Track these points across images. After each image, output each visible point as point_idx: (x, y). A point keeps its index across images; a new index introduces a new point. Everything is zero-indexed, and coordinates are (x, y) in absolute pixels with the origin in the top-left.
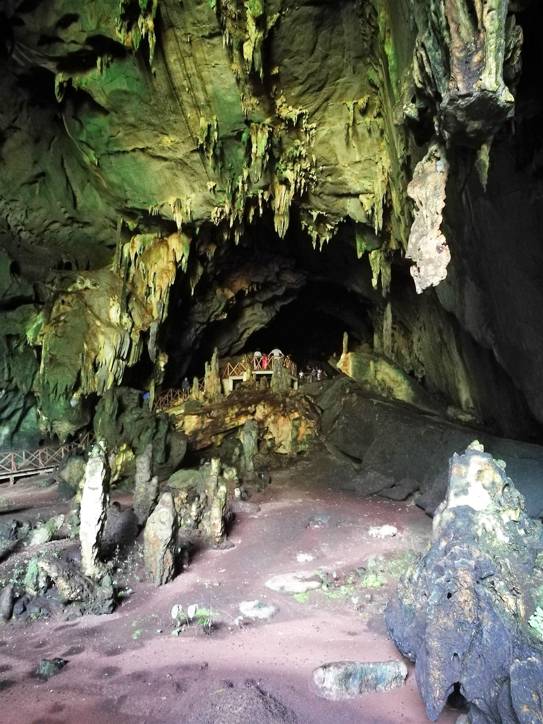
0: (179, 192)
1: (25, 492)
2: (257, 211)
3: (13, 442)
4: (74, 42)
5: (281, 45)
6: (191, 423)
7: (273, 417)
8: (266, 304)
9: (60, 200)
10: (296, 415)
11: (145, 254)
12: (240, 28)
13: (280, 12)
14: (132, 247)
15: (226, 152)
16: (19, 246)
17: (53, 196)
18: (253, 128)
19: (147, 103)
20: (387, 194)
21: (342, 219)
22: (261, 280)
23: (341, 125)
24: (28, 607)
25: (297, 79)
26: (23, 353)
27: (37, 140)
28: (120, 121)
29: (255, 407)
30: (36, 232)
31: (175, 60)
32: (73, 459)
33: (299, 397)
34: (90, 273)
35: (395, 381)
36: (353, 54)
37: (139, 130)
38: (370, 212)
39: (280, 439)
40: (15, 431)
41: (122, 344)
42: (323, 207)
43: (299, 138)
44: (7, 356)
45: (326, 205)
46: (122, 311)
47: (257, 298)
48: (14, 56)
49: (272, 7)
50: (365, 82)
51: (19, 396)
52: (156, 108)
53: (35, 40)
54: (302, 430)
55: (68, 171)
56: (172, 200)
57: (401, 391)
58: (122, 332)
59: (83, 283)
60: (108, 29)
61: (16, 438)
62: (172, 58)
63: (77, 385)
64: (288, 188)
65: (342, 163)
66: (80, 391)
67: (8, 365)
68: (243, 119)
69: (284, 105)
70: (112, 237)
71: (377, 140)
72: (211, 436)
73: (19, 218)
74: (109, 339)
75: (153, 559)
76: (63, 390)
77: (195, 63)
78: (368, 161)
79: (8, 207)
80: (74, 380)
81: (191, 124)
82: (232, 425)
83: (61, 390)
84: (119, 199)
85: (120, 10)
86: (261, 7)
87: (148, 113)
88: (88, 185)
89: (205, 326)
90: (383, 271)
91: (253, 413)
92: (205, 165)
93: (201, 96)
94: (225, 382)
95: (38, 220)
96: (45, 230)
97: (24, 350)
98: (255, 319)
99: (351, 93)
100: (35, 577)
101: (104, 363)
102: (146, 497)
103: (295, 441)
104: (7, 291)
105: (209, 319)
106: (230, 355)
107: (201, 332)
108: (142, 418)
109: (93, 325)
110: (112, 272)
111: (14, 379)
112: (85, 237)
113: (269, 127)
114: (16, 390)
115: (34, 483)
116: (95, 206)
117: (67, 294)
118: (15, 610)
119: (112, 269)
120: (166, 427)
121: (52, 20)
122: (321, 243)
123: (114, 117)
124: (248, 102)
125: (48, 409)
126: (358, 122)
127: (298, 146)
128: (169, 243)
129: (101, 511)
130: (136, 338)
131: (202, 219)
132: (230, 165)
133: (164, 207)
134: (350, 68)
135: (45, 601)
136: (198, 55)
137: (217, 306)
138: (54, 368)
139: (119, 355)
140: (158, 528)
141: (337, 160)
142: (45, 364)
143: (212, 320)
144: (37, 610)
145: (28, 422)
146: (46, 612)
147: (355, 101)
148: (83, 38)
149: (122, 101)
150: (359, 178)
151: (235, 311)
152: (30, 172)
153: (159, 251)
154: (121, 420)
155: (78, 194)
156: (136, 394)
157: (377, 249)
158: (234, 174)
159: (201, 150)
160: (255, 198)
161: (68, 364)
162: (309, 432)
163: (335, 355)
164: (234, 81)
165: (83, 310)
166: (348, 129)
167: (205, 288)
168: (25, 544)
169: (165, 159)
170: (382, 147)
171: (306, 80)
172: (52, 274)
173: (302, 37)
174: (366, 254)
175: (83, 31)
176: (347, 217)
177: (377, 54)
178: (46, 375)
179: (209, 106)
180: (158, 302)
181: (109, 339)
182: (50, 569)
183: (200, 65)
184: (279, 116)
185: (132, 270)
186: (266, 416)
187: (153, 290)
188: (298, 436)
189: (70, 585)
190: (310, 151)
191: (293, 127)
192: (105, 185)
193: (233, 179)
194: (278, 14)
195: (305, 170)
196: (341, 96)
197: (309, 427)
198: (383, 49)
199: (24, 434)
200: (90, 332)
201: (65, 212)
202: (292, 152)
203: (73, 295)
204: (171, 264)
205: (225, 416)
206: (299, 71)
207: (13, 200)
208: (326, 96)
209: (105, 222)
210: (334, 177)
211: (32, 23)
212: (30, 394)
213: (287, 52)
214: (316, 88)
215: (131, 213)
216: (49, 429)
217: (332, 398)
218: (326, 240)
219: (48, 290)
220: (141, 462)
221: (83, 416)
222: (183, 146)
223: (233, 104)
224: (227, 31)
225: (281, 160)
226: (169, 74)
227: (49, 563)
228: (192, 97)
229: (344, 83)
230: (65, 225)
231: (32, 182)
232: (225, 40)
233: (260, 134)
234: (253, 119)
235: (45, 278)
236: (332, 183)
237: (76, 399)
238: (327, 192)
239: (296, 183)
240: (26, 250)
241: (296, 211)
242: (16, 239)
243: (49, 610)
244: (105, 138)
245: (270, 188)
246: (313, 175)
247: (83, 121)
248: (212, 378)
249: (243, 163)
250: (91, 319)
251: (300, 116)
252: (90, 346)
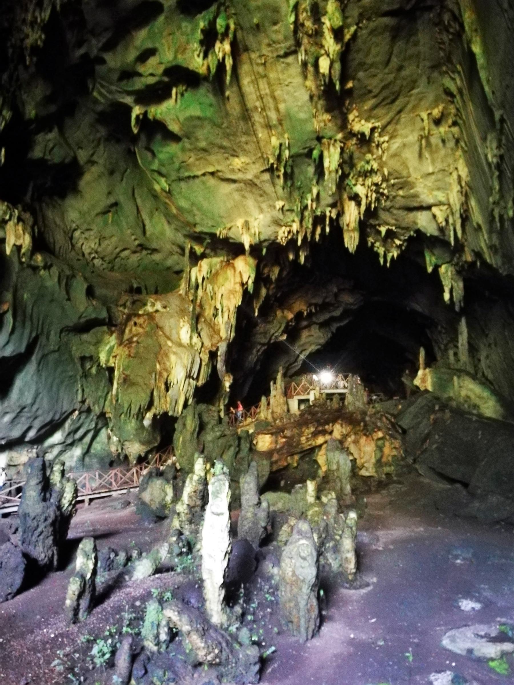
0: (248, 213)
1: (100, 514)
2: (323, 229)
3: (85, 463)
4: (152, 75)
5: (357, 57)
6: (264, 442)
7: (353, 437)
8: (323, 325)
9: (131, 227)
10: (380, 434)
11: (213, 277)
12: (316, 44)
13: (357, 24)
14: (200, 271)
15: (296, 171)
16: (93, 272)
17: (124, 224)
18: (324, 144)
19: (219, 126)
20: (465, 204)
21: (412, 233)
22: (319, 300)
23: (414, 137)
24: (149, 667)
25: (370, 92)
26: (96, 375)
27: (112, 173)
28: (192, 147)
29: (333, 425)
30: (107, 259)
31: (249, 83)
32: (155, 480)
33: (379, 416)
34: (159, 297)
35: (479, 397)
36: (428, 64)
37: (210, 154)
38: (444, 224)
39: (363, 461)
40: (87, 452)
41: (192, 363)
42: (393, 222)
43: (370, 152)
44: (81, 377)
45: (396, 220)
46: (192, 331)
47: (314, 319)
48: (95, 94)
49: (349, 20)
50: (441, 91)
51: (91, 417)
52: (228, 130)
53: (115, 76)
54: (387, 450)
55: (139, 201)
56: (240, 222)
57: (488, 408)
58: (193, 352)
59: (153, 305)
60: (185, 59)
61: (87, 459)
62: (246, 81)
63: (151, 404)
64: (359, 204)
65: (414, 176)
66: (153, 411)
67: (82, 386)
68: (315, 136)
69: (356, 119)
70: (178, 263)
71: (452, 149)
72: (287, 457)
73: (92, 245)
74: (181, 358)
75: (292, 604)
76: (137, 410)
77: (269, 83)
78: (441, 172)
79: (83, 236)
80: (148, 399)
81: (262, 144)
82: (309, 445)
83: (135, 410)
84: (188, 224)
85: (199, 35)
86: (340, 18)
87: (219, 137)
88: (157, 213)
89: (266, 347)
90: (455, 285)
91: (331, 433)
92: (274, 184)
93: (273, 116)
94: (290, 401)
95: (110, 248)
96: (116, 258)
97: (97, 372)
98: (312, 339)
99: (424, 104)
100: (155, 627)
101: (175, 383)
102: (255, 523)
103: (379, 463)
104: (83, 313)
105: (270, 339)
106: (293, 375)
107: (262, 353)
108: (225, 436)
109: (164, 346)
110: (180, 295)
111: (87, 401)
112: (154, 263)
113: (341, 142)
114: (89, 411)
115: (109, 504)
116: (163, 233)
117: (139, 316)
118: (135, 672)
119: (181, 292)
120: (248, 445)
121: (132, 55)
122: (389, 259)
123: (186, 144)
124: (320, 118)
125: (120, 430)
126: (432, 132)
127: (370, 160)
128: (236, 265)
129: (228, 542)
130: (206, 357)
131: (269, 240)
132: (299, 183)
133: (233, 229)
134: (424, 79)
135: (169, 659)
136: (272, 75)
137: (278, 328)
138: (127, 387)
139: (190, 374)
140: (298, 564)
141: (409, 172)
142: (118, 384)
143: (272, 341)
144: (161, 673)
145: (98, 443)
146: (172, 677)
147: (429, 112)
148: (161, 69)
149: (195, 127)
150: (432, 190)
151: (293, 332)
152: (105, 202)
153: (226, 272)
154: (202, 438)
155: (147, 222)
156: (215, 411)
157: (447, 263)
158: (303, 193)
159: (271, 170)
160: (324, 216)
161: (142, 383)
162: (395, 453)
163: (407, 372)
164: (307, 97)
165: (155, 332)
166: (421, 141)
167: (267, 310)
168: (127, 577)
169: (234, 181)
170: (457, 157)
171: (380, 92)
172: (125, 298)
173: (377, 49)
174: (437, 267)
175: (161, 63)
176: (418, 231)
177: (454, 61)
178: (120, 395)
179: (281, 124)
180: (227, 323)
181: (181, 358)
182: (180, 620)
183: (274, 85)
184: (351, 130)
185: (200, 292)
186: (345, 437)
187: (220, 311)
188: (382, 457)
189: (206, 642)
190: (382, 165)
191: (365, 141)
192: (174, 211)
193: (302, 197)
194: (355, 27)
195: (376, 185)
196: (414, 108)
197: (395, 448)
198: (470, 49)
199: (95, 455)
200: (162, 352)
201: (135, 239)
202: (363, 166)
203: (146, 317)
204: (238, 285)
205: (301, 435)
206: (374, 84)
207: (88, 230)
208: (398, 109)
209: (172, 248)
210: (405, 190)
211: (114, 61)
212: (102, 415)
213: (362, 64)
214: (389, 100)
215: (198, 238)
216: (120, 451)
217: (416, 416)
218: (393, 256)
219: (121, 313)
220: (246, 482)
221: (153, 436)
222: (253, 166)
223: (305, 121)
224: (303, 48)
225: (352, 175)
226: (242, 95)
227: (179, 613)
228: (264, 117)
229: (418, 93)
230: (135, 252)
231: (105, 212)
232: (301, 56)
233: (332, 149)
234: (324, 135)
235: (117, 301)
236: (403, 197)
237: (149, 418)
238: (397, 206)
239: (367, 197)
240: (100, 276)
241: (364, 226)
242: (91, 265)
243: (175, 673)
244: (177, 165)
245: (339, 205)
246: (384, 189)
247: (156, 151)
248: (278, 397)
249: (312, 180)
250: (162, 339)
251: (373, 130)
252: (162, 365)
